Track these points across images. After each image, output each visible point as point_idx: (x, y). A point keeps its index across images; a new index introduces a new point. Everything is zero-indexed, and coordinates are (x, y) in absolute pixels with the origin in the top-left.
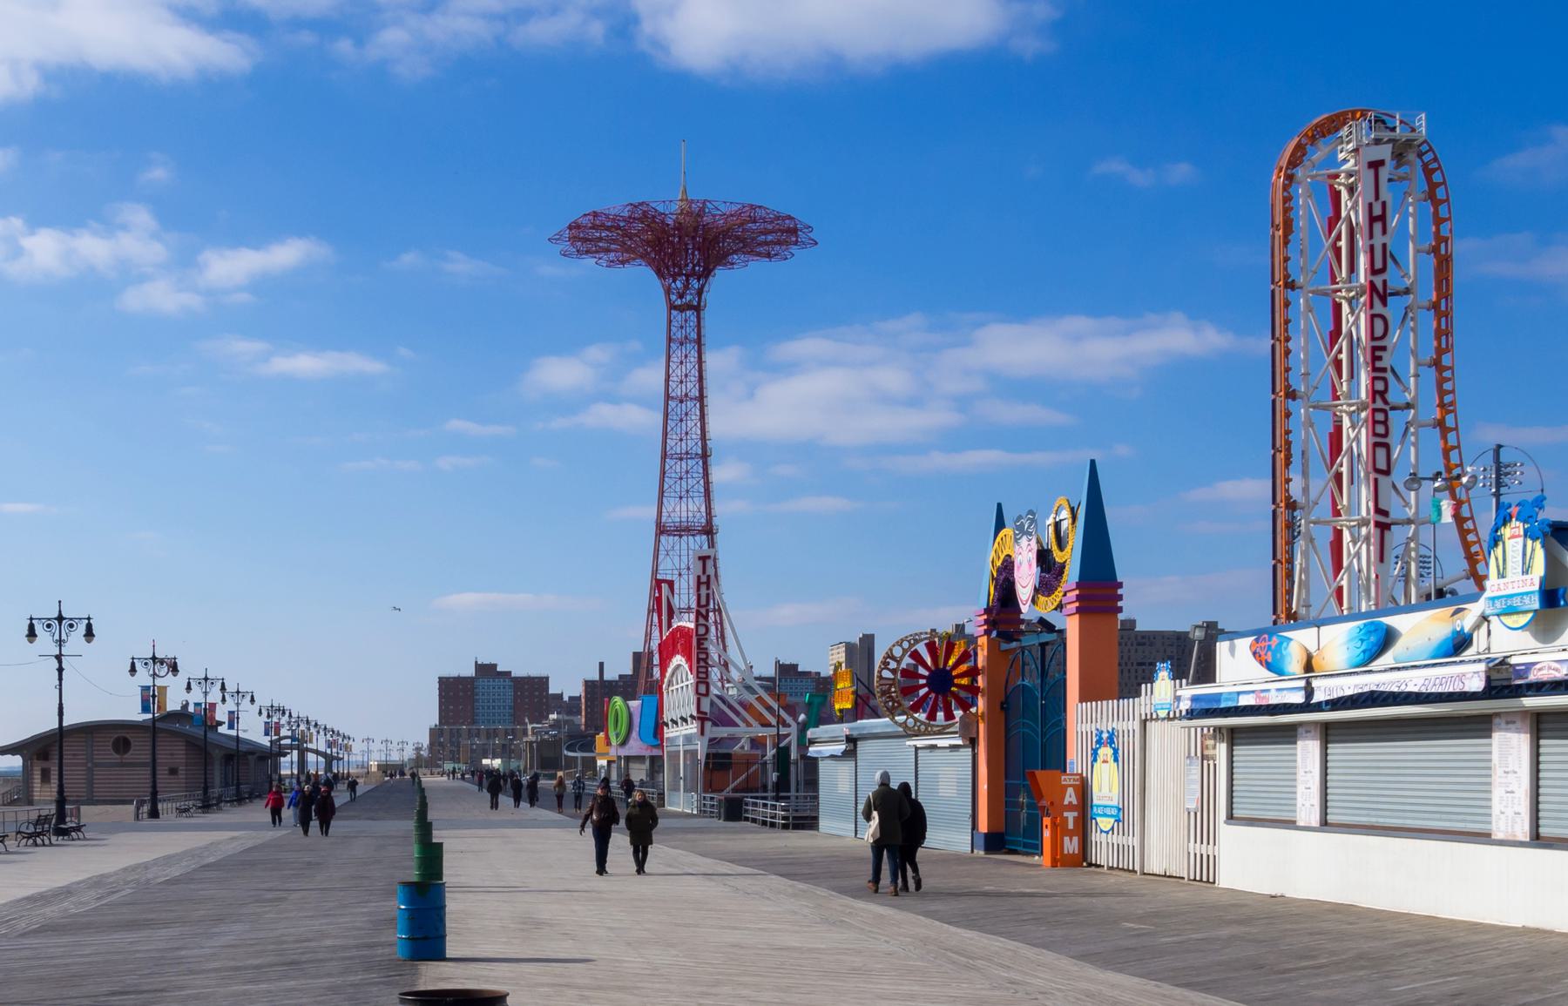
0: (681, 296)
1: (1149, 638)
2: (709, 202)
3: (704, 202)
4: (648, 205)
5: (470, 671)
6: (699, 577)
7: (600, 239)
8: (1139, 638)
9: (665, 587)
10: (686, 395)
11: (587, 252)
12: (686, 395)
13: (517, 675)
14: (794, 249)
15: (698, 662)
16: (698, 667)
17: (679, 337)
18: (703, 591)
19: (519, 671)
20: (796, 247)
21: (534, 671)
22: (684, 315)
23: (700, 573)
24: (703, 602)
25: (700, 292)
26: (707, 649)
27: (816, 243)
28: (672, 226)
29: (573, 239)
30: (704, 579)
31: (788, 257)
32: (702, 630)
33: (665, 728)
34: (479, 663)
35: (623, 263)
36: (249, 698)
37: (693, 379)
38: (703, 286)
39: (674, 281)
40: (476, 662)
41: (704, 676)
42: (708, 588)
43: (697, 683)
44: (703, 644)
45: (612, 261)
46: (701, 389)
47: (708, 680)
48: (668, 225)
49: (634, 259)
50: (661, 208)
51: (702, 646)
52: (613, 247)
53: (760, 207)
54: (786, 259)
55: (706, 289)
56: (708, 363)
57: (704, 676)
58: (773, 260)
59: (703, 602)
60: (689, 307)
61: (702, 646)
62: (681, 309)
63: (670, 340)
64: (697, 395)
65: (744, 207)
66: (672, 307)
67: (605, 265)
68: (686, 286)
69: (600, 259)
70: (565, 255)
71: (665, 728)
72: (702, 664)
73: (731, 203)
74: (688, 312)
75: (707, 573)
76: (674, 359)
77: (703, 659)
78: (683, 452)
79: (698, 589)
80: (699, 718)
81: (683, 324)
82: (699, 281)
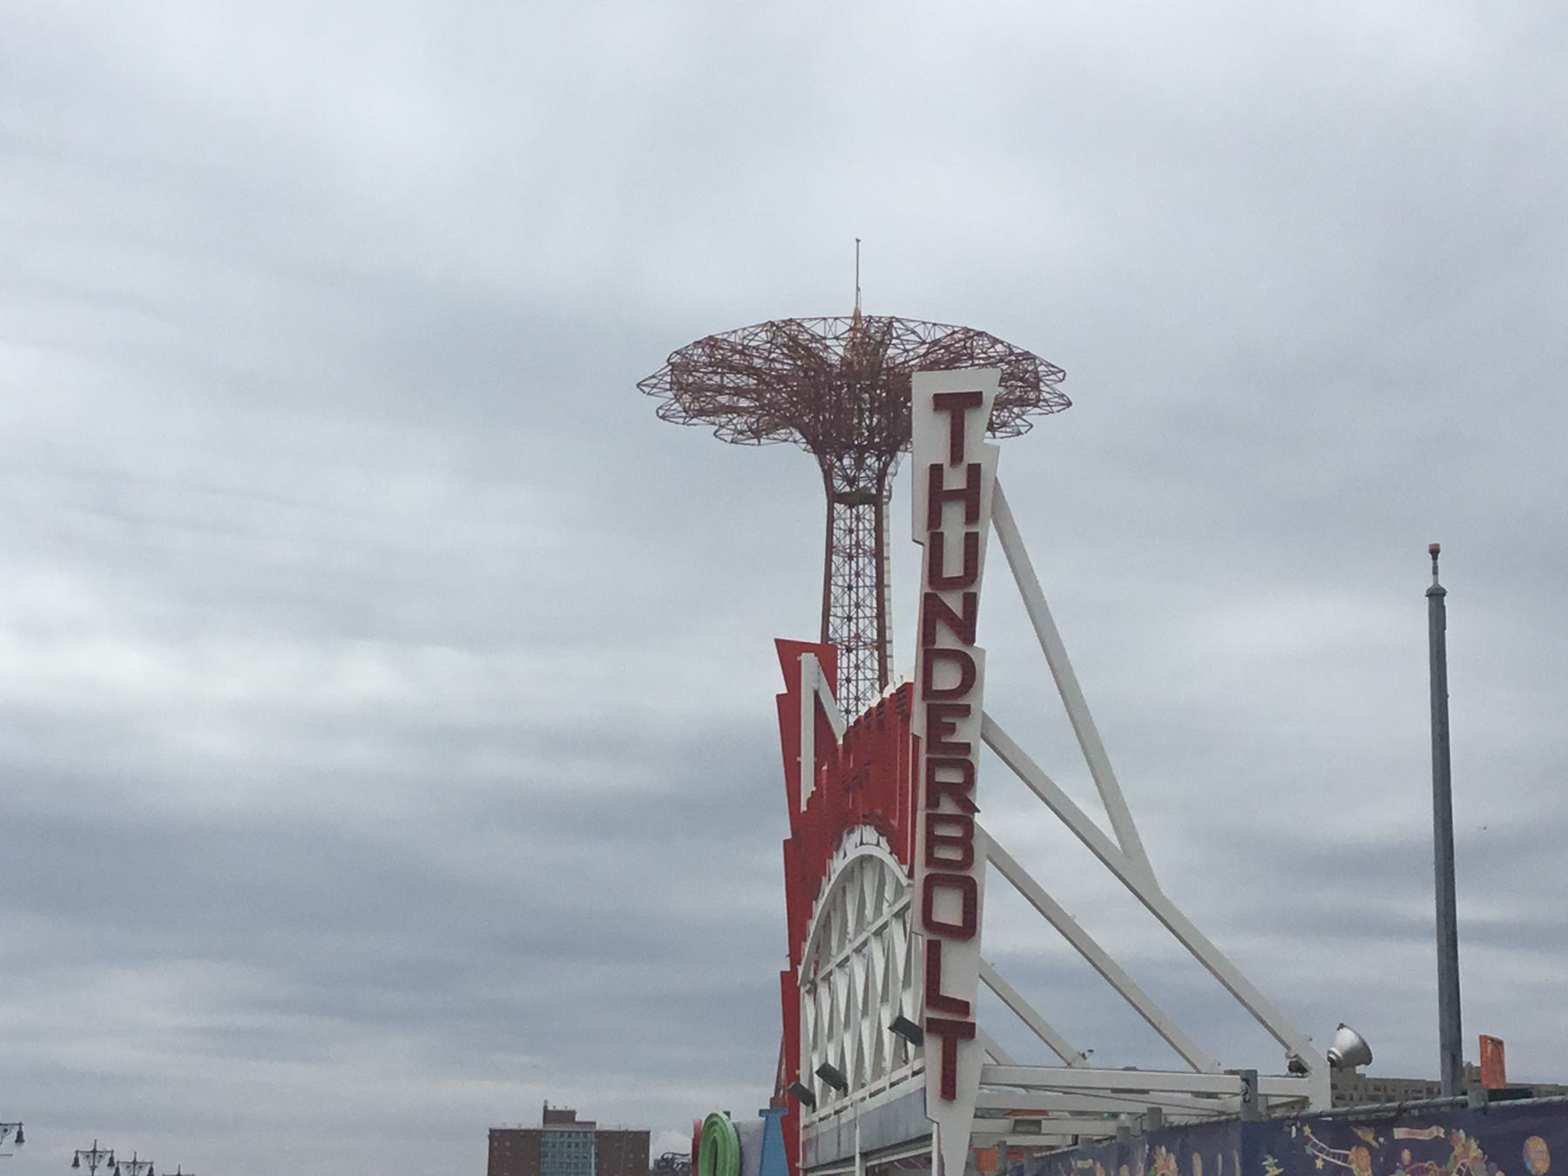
0: (851, 481)
1: (1385, 1090)
2: (898, 320)
3: (891, 321)
4: (799, 325)
5: (535, 1122)
6: (936, 471)
7: (720, 389)
8: (1371, 1088)
9: (808, 661)
10: (857, 636)
11: (701, 413)
12: (857, 636)
13: (606, 1128)
14: (1032, 414)
15: (932, 802)
16: (932, 820)
17: (845, 634)
18: (954, 525)
19: (605, 1123)
20: (1037, 410)
21: (630, 1122)
22: (854, 510)
23: (942, 457)
24: (953, 567)
25: (881, 476)
26: (967, 747)
27: (1069, 404)
28: (836, 371)
29: (679, 387)
30: (955, 480)
31: (1023, 430)
32: (947, 677)
33: (802, 1107)
34: (550, 1108)
35: (757, 434)
36: (13, 1135)
37: (869, 674)
38: (886, 465)
39: (840, 459)
40: (545, 1107)
41: (954, 855)
42: (972, 516)
43: (930, 884)
44: (952, 729)
45: (741, 433)
46: (881, 630)
47: (972, 874)
48: (830, 366)
49: (776, 427)
50: (819, 330)
51: (946, 739)
52: (744, 403)
53: (980, 334)
54: (1019, 433)
55: (891, 470)
56: (893, 589)
57: (954, 855)
58: (997, 434)
59: (953, 567)
60: (861, 498)
61: (946, 739)
62: (851, 501)
63: (830, 549)
64: (875, 637)
65: (954, 332)
66: (834, 497)
67: (729, 438)
68: (859, 464)
69: (722, 427)
70: (663, 417)
71: (802, 1107)
72: (948, 807)
73: (935, 325)
74: (861, 507)
75: (970, 458)
76: (839, 523)
77: (950, 788)
78: (854, 652)
79: (934, 519)
80: (933, 1026)
81: (853, 614)
82: (879, 459)
